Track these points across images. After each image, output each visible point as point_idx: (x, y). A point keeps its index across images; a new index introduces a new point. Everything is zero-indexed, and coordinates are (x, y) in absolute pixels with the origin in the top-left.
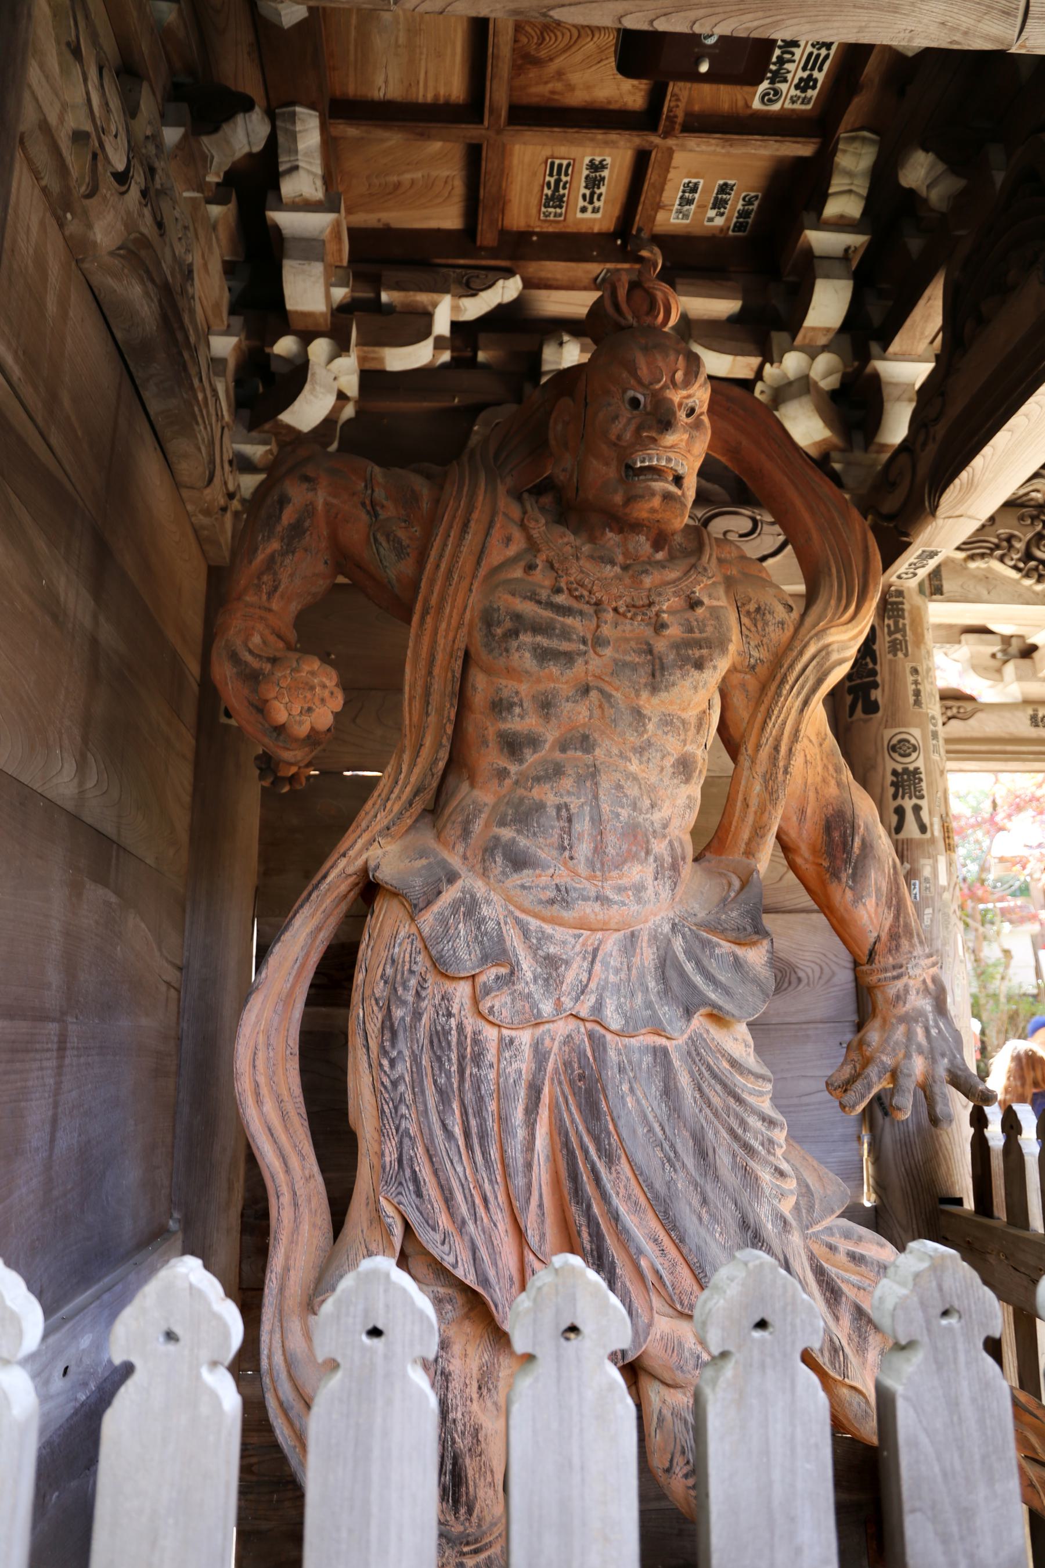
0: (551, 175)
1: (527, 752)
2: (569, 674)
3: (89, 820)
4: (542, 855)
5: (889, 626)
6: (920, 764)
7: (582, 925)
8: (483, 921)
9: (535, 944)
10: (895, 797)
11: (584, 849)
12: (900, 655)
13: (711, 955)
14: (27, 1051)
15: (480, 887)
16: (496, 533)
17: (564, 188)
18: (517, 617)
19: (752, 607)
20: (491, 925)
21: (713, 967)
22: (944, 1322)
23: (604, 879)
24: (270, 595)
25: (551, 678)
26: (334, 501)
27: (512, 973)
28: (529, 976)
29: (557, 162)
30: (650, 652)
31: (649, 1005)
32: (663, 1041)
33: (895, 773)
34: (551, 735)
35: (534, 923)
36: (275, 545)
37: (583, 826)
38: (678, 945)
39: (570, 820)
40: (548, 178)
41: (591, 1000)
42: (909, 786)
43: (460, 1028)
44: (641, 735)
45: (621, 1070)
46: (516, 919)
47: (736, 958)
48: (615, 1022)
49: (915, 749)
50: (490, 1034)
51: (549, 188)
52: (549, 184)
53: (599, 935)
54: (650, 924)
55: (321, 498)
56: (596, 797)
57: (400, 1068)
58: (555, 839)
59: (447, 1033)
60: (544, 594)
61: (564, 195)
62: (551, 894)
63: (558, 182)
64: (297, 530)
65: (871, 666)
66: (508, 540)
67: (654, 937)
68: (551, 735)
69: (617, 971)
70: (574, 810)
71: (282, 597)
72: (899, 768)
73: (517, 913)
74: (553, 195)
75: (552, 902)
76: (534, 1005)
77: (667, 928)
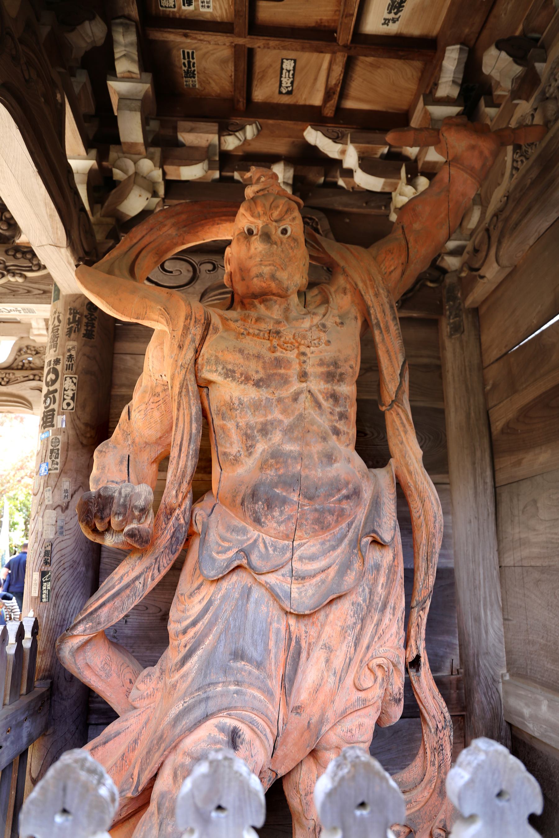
0: (184, 58)
17: (194, 66)
22: (358, 813)
29: (186, 51)
40: (183, 61)
51: (185, 66)
52: (184, 64)
61: (194, 71)
63: (189, 62)
74: (188, 70)
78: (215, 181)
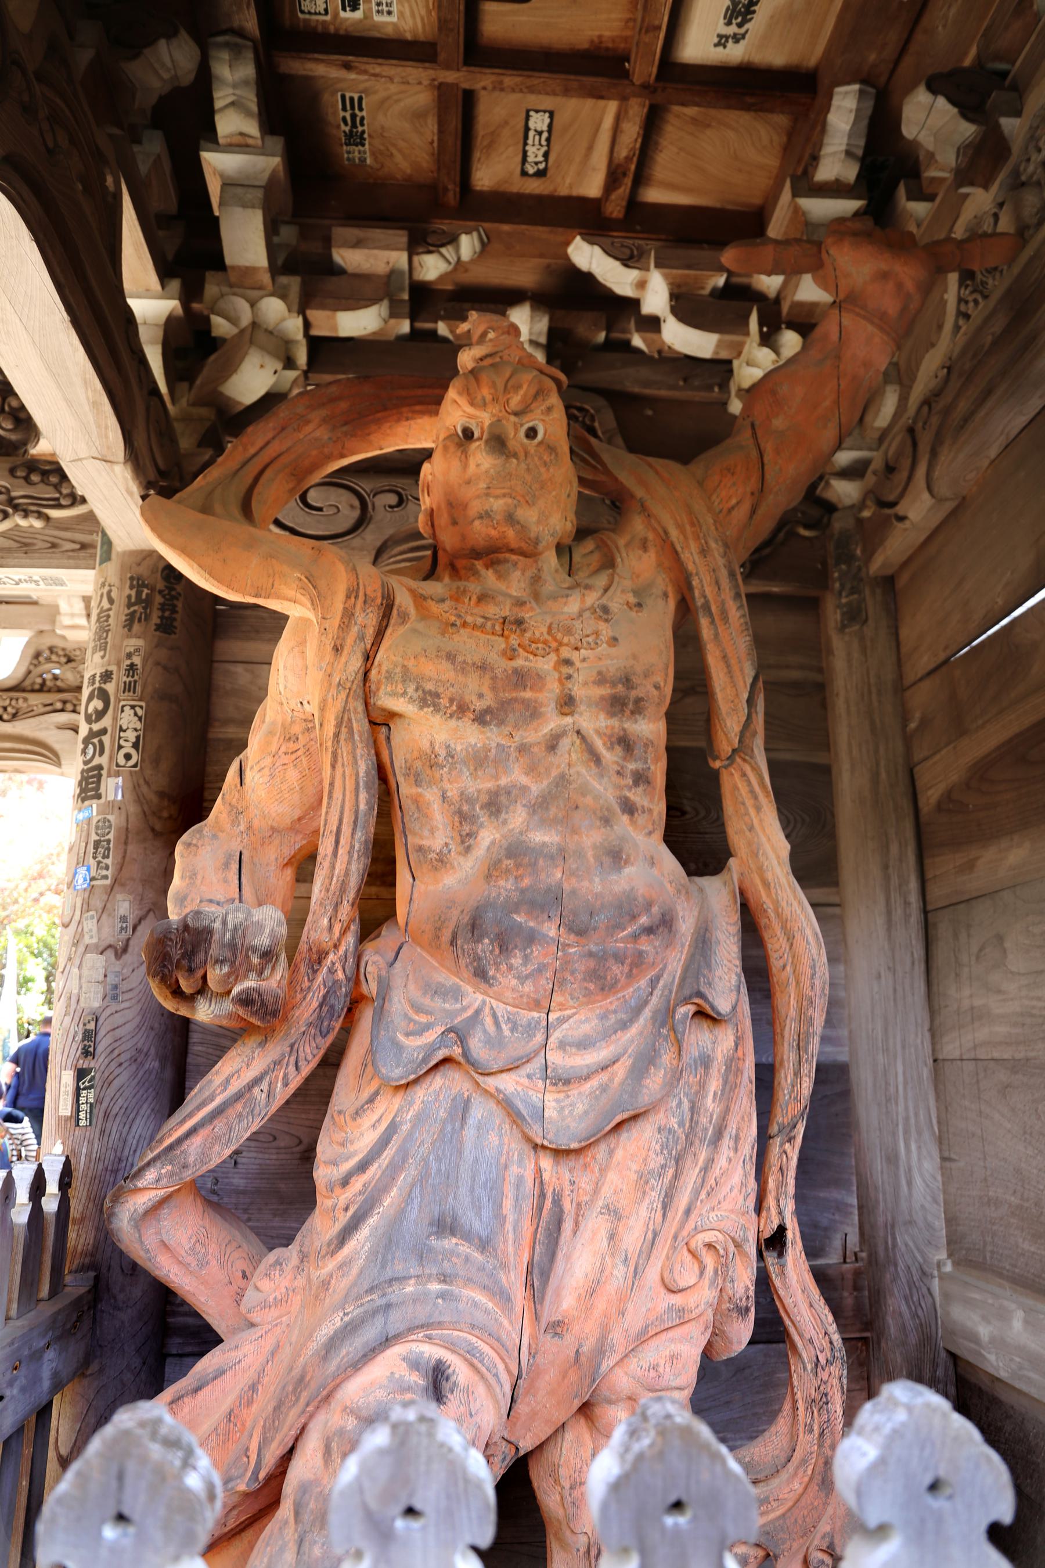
0: (344, 109)
14: (125, 1141)
17: (362, 124)
22: (670, 1521)
29: (348, 95)
40: (342, 114)
51: (346, 124)
52: (344, 119)
61: (363, 132)
63: (354, 116)
74: (351, 131)
78: (401, 338)
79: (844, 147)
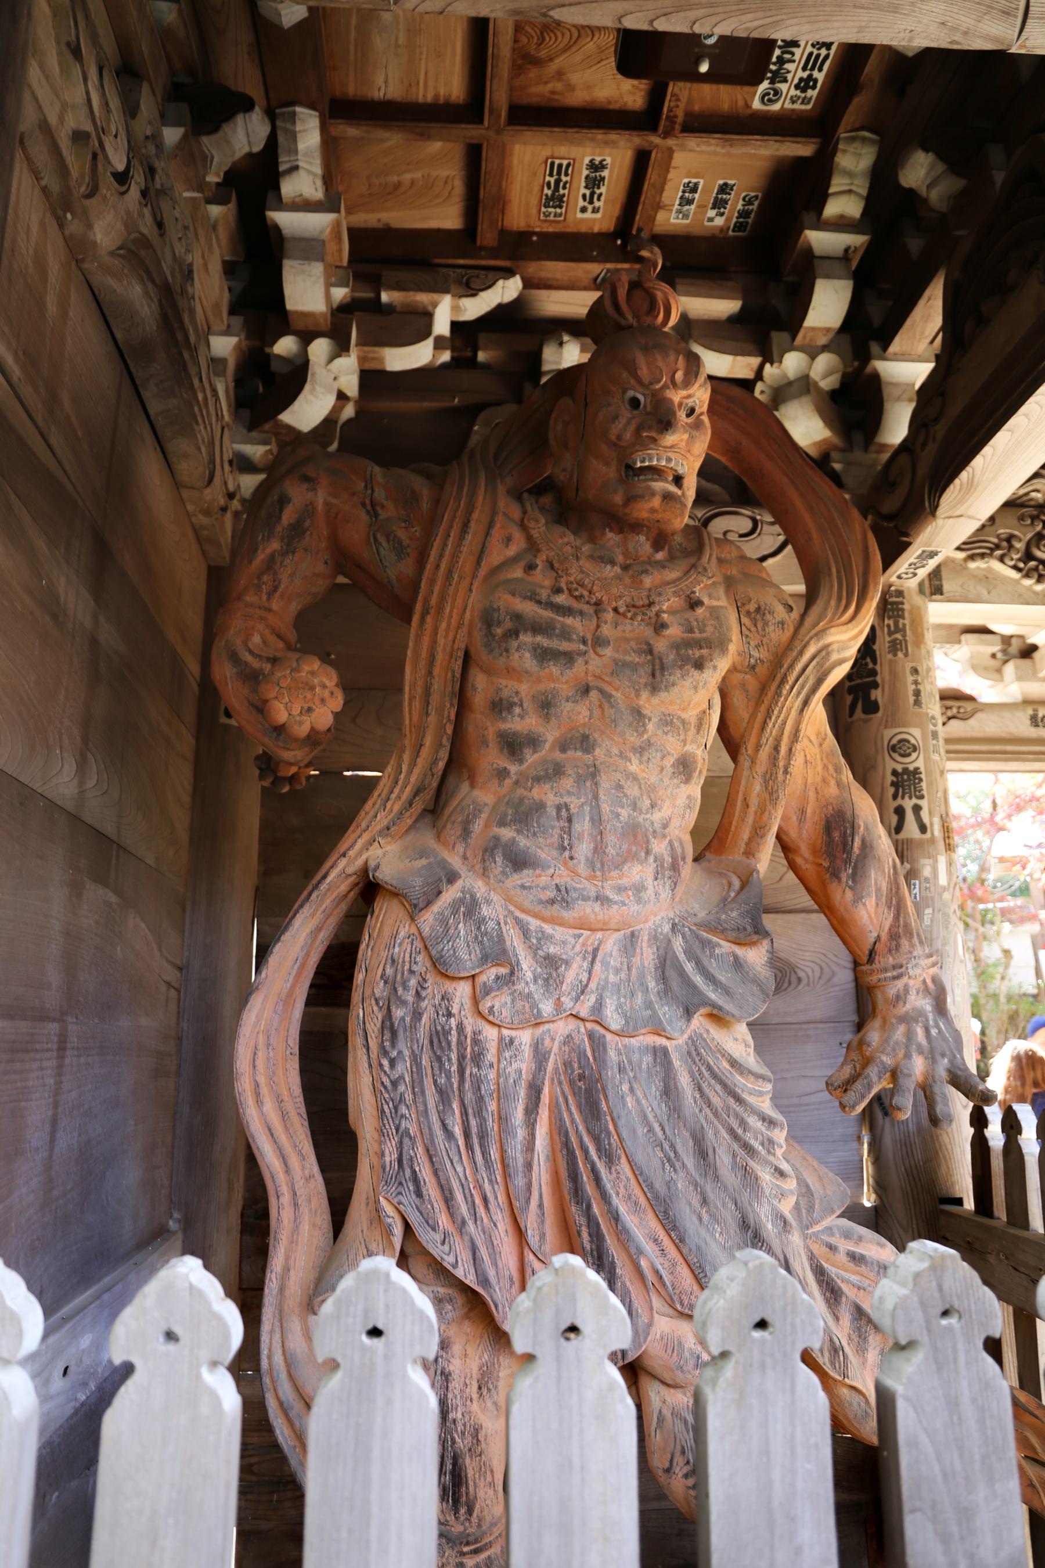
0: (551, 175)
1: (527, 752)
2: (569, 674)
3: (89, 820)
4: (542, 855)
5: (889, 626)
6: (920, 764)
7: (582, 925)
8: (483, 921)
9: (535, 944)
10: (895, 797)
11: (584, 849)
12: (900, 655)
13: (711, 955)
14: (27, 1051)
15: (480, 887)
16: (496, 533)
17: (564, 188)
18: (517, 617)
19: (752, 607)
20: (491, 925)
21: (713, 967)
23: (604, 879)
24: (270, 595)
25: (551, 678)
26: (334, 501)
27: (512, 973)
28: (529, 976)
29: (557, 162)
30: (650, 652)
31: (649, 1005)
32: (663, 1041)
33: (895, 773)
34: (551, 735)
35: (534, 923)
36: (275, 545)
37: (583, 826)
38: (678, 945)
39: (570, 820)
40: (548, 178)
41: (591, 1000)
42: (909, 786)
43: (460, 1028)
44: (641, 735)
45: (621, 1070)
46: (516, 919)
47: (736, 958)
48: (615, 1022)
49: (915, 749)
50: (490, 1034)
51: (549, 188)
52: (549, 184)
53: (599, 935)
54: (650, 924)
55: (321, 498)
56: (596, 797)
57: (400, 1068)
58: (555, 839)
59: (447, 1033)
60: (544, 594)
61: (564, 195)
62: (551, 894)
63: (558, 182)
64: (297, 530)
65: (871, 666)
66: (508, 540)
67: (654, 937)
68: (551, 735)
69: (617, 971)
70: (574, 810)
71: (282, 597)
72: (899, 768)
73: (517, 913)
74: (553, 195)
75: (552, 902)
76: (534, 1005)
77: (667, 928)
78: (444, 366)
79: (884, 1282)
